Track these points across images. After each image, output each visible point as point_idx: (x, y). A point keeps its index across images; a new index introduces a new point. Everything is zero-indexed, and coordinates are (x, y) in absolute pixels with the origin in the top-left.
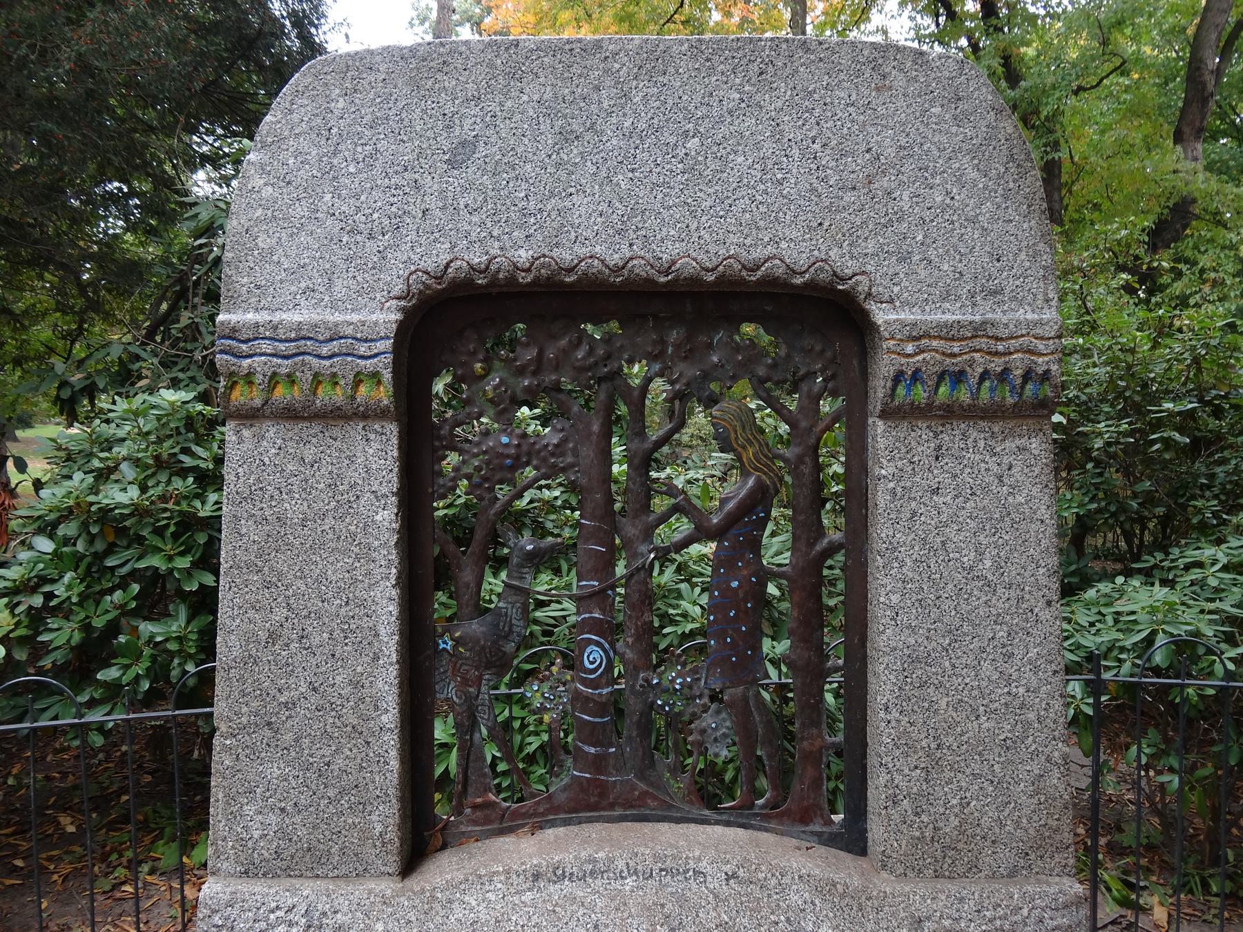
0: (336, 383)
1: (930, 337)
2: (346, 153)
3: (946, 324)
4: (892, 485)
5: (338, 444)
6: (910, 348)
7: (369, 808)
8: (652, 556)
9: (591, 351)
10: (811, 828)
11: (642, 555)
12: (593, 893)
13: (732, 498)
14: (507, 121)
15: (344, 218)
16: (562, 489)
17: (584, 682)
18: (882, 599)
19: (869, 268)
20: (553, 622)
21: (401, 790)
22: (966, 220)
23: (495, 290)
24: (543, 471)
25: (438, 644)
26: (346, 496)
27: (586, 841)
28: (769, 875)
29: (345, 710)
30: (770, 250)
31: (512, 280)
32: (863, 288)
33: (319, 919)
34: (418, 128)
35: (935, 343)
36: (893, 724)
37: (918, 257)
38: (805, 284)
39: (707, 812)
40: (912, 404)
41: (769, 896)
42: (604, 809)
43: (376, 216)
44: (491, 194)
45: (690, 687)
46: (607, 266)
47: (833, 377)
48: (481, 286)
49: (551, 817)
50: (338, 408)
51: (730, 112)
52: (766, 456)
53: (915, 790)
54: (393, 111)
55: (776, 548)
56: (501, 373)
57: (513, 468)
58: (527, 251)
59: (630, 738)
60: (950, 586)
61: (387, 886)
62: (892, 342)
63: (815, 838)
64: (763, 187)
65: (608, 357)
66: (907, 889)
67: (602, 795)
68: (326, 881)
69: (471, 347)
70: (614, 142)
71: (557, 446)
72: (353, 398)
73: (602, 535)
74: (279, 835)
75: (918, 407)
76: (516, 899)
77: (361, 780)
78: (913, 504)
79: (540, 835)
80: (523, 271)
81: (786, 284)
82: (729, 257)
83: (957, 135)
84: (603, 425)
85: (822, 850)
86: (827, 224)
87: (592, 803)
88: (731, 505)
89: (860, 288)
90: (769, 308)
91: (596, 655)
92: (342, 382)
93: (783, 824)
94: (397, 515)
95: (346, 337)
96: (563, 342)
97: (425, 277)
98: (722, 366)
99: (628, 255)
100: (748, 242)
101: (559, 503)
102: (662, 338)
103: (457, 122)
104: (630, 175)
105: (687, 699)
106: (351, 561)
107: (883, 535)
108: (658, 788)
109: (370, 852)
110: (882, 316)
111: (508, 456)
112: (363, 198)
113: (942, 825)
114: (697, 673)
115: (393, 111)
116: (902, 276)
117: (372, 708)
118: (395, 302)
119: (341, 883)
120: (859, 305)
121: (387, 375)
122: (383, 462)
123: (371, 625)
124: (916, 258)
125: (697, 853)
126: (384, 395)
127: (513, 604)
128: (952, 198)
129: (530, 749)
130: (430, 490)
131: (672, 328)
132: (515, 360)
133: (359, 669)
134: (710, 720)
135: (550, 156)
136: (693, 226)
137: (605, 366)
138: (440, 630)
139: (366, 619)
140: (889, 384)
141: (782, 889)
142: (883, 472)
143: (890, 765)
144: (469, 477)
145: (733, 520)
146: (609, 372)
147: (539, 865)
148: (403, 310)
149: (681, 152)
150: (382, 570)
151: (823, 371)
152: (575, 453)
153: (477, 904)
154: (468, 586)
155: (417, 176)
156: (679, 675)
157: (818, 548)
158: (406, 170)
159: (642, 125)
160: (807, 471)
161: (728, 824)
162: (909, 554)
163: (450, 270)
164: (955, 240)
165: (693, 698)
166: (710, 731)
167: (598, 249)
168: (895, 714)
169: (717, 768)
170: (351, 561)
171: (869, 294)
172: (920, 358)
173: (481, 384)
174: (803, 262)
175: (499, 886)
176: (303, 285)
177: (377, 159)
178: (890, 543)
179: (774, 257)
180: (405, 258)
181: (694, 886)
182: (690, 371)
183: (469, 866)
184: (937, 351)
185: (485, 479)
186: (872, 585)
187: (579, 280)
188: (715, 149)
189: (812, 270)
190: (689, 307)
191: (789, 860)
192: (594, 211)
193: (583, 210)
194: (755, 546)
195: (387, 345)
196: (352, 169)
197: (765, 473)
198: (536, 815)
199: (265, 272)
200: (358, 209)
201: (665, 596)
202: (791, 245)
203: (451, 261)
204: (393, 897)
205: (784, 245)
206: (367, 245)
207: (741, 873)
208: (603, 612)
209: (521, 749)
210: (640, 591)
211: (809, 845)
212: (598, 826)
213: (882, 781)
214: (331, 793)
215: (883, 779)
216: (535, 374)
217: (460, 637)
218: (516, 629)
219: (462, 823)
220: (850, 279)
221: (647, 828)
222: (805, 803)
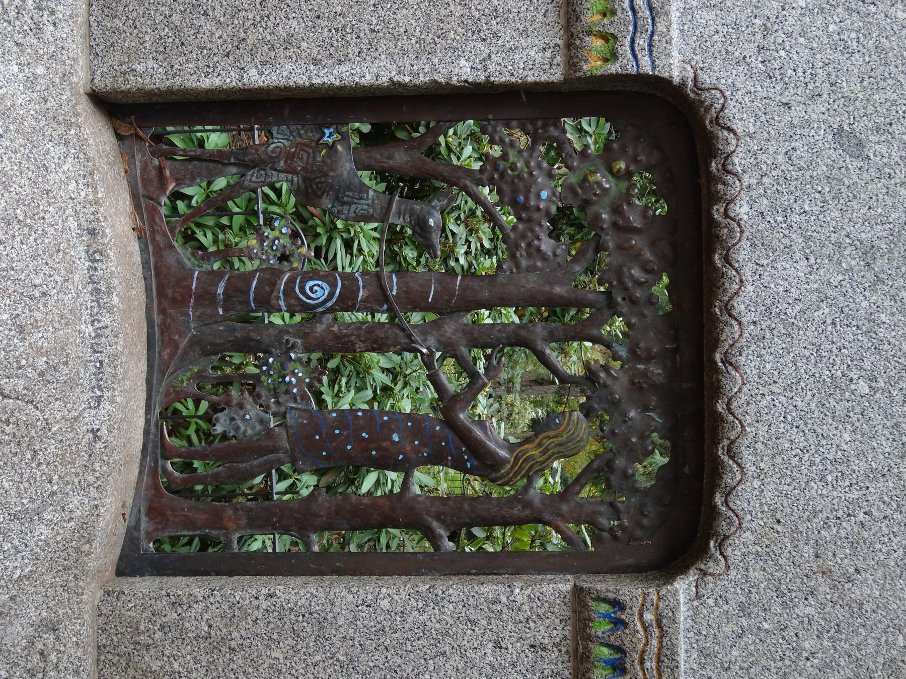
0: (605, 15)
1: (661, 638)
2: (848, 22)
3: (675, 653)
4: (504, 599)
5: (540, 18)
6: (649, 616)
7: (160, 57)
8: (425, 351)
9: (639, 284)
10: (144, 518)
11: (425, 340)
12: (75, 293)
13: (486, 434)
14: (884, 191)
15: (780, 20)
16: (466, 266)
17: (291, 281)
18: (384, 590)
19: (733, 573)
20: (330, 257)
21: (179, 91)
22: (785, 674)
23: (703, 181)
24: (512, 235)
25: (329, 128)
26: (485, 27)
27: (128, 285)
28: (97, 474)
29: (261, 30)
30: (751, 469)
31: (715, 198)
32: (711, 567)
33: (48, 7)
34: (876, 97)
35: (655, 642)
36: (255, 602)
37: (745, 624)
38: (714, 507)
39: (158, 411)
40: (590, 620)
41: (77, 474)
42: (160, 303)
43: (783, 53)
44: (807, 175)
45: (287, 392)
46: (731, 298)
47: (615, 538)
48: (708, 165)
49: (151, 249)
51: (897, 425)
52: (530, 468)
53: (187, 625)
54: (894, 70)
55: (436, 481)
56: (614, 189)
57: (514, 203)
59: (234, 330)
60: (399, 661)
61: (80, 79)
62: (655, 598)
63: (133, 523)
64: (818, 460)
65: (633, 302)
66: (86, 617)
67: (174, 302)
68: (85, 14)
69: (642, 158)
70: (864, 304)
71: (538, 249)
72: (590, 33)
73: (445, 297)
75: (586, 626)
76: (70, 211)
77: (190, 48)
78: (484, 622)
79: (133, 236)
80: (726, 210)
81: (714, 487)
82: (742, 426)
83: (874, 662)
84: (561, 297)
85: (122, 531)
86: (779, 528)
87: (167, 291)
88: (479, 433)
89: (711, 564)
90: (686, 470)
91: (319, 293)
92: (606, 21)
93: (147, 489)
94: (466, 81)
95: (654, 24)
96: (648, 255)
97: (718, 107)
98: (625, 422)
99: (744, 320)
100: (760, 446)
101: (452, 263)
102: (653, 358)
103: (884, 138)
104: (829, 321)
105: (275, 389)
106: (417, 34)
107: (451, 591)
108: (182, 359)
109: (115, 59)
110: (683, 587)
111: (527, 198)
112: (801, 40)
113: (152, 652)
114: (302, 399)
115: (894, 70)
116: (725, 607)
117: (264, 58)
118: (691, 75)
119: (84, 30)
120: (693, 564)
121: (614, 68)
122: (522, 65)
123: (350, 56)
124: (744, 622)
125: (118, 399)
126: (593, 65)
127: (372, 206)
128: (808, 659)
129: (200, 235)
130: (490, 117)
131: (665, 368)
133: (304, 45)
134: (252, 413)
135: (848, 236)
136: (775, 388)
137: (624, 299)
138: (344, 129)
139: (357, 50)
140: (611, 596)
141: (84, 488)
142: (517, 591)
143: (212, 600)
144: (504, 157)
145: (463, 435)
146: (617, 303)
147: (104, 235)
148: (683, 84)
149: (854, 374)
150: (408, 67)
151: (621, 526)
152: (531, 269)
153: (64, 170)
154: (390, 157)
155: (825, 96)
156: (299, 380)
157: (435, 524)
158: (832, 85)
159: (882, 332)
160: (515, 511)
161: (146, 432)
162: (431, 618)
163: (726, 133)
164: (764, 662)
165: (276, 396)
166: (242, 413)
167: (750, 288)
168: (265, 604)
169: (182, 431)
170: (417, 34)
171: (705, 574)
172: (639, 627)
173: (603, 169)
174: (738, 503)
175: (83, 194)
177: (843, 54)
178: (443, 599)
179: (743, 474)
180: (739, 85)
181: (86, 397)
182: (619, 389)
183: (102, 163)
184: (646, 644)
185: (502, 175)
186: (399, 580)
187: (716, 269)
188: (858, 410)
189: (730, 513)
190: (685, 386)
191: (113, 495)
192: (790, 284)
193: (791, 272)
194: (437, 458)
195: (646, 67)
196: (832, 28)
197: (512, 468)
198: (153, 232)
200: (789, 35)
201: (358, 373)
202: (757, 490)
203: (735, 134)
204: (71, 84)
205: (757, 483)
206: (752, 46)
207: (99, 445)
208: (365, 300)
209: (199, 225)
210: (387, 338)
211: (127, 516)
212: (143, 297)
213: (196, 591)
214: (176, 18)
215: (198, 592)
216: (615, 225)
217: (336, 151)
218: (346, 208)
219: (143, 155)
220: (721, 553)
221: (141, 348)
222: (169, 513)
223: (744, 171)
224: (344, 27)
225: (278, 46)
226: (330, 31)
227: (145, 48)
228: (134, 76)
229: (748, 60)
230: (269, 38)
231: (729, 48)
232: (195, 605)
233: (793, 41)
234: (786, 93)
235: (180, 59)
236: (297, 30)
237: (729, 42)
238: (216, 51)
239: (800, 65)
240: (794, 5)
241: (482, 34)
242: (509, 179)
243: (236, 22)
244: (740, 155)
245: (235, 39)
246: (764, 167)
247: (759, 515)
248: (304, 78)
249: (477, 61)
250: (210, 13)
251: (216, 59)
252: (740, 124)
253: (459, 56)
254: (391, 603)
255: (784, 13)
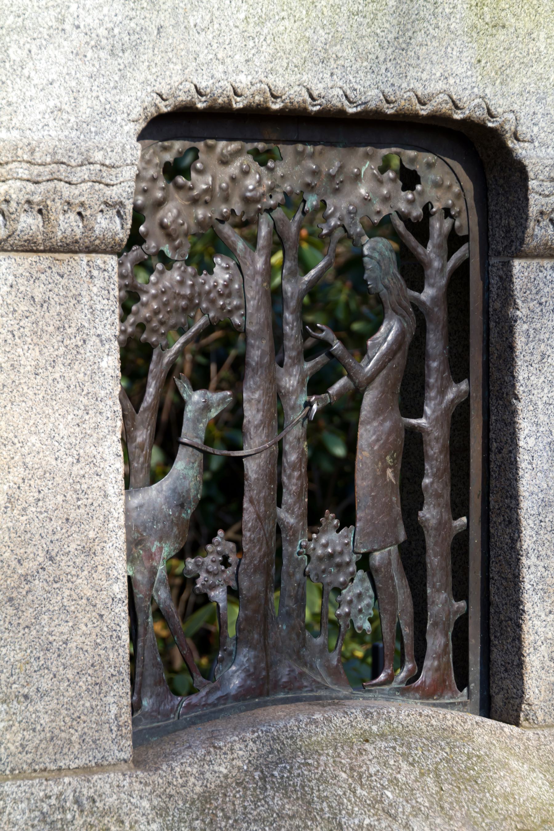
5: (64, 281)
7: (105, 688)
19: (516, 107)
26: (73, 340)
30: (441, 86)
44: (217, 13)
50: (77, 242)
58: (247, 76)
74: (23, 725)
77: (97, 658)
86: (483, 62)
89: (507, 127)
111: (184, 297)
122: (106, 302)
123: (100, 484)
132: (191, 189)
150: (110, 422)
170: (80, 413)
175: (241, 753)
176: (51, 104)
178: (526, 386)
199: (16, 87)
205: (451, 81)
223: (212, 77)
224: (75, 491)
225: (92, 562)
226: (79, 507)
227: (97, 706)
228: (121, 716)
229: (122, 67)
230: (86, 573)
231: (112, 85)
232: (536, 628)
233: (106, 18)
234: (150, 29)
235: (106, 666)
236: (79, 543)
237: (107, 86)
238: (98, 629)
239: (127, 13)
240: (75, 16)
241: (80, 344)
242: (167, 316)
243: (73, 608)
244: (200, 79)
245: (87, 609)
246: (211, 56)
247: (474, 79)
248: (120, 533)
249: (102, 349)
250: (66, 637)
251: (105, 629)
252: (174, 79)
253: (99, 368)
254: (530, 437)
255: (82, 26)
